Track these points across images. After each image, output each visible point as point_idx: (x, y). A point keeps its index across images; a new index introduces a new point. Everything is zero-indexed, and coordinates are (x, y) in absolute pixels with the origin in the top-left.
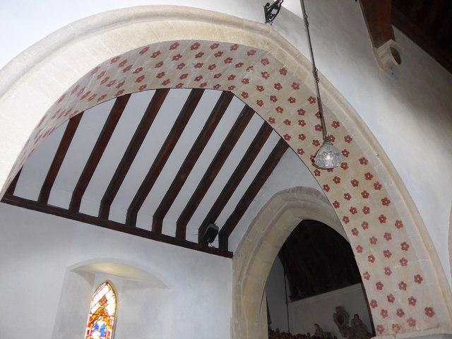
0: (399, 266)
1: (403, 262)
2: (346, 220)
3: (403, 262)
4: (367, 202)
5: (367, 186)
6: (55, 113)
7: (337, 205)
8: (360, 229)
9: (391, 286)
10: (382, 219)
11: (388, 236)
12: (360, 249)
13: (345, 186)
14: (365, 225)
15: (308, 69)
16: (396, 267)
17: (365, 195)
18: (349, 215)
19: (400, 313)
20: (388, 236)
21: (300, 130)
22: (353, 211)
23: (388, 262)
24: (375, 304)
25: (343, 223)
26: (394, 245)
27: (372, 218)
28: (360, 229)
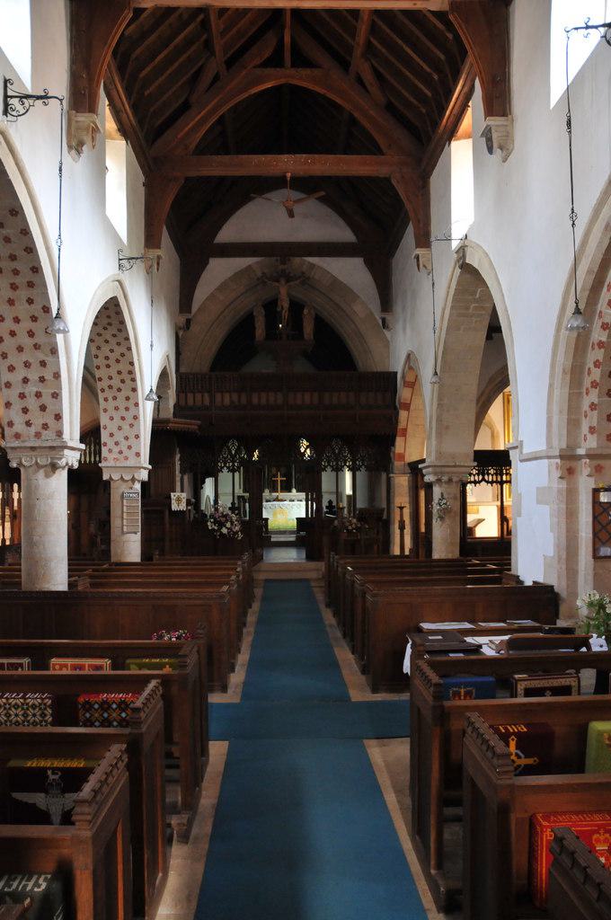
0: (128, 427)
1: (131, 425)
2: (103, 390)
3: (131, 425)
4: (121, 385)
5: (125, 376)
6: (398, 308)
7: (100, 379)
8: (110, 399)
9: (119, 436)
10: (128, 399)
11: (127, 409)
12: (105, 428)
13: (113, 372)
14: (115, 398)
15: (491, 428)
16: (126, 427)
17: (123, 381)
18: (107, 389)
19: (121, 452)
20: (127, 409)
21: (115, 431)
22: (110, 387)
23: (121, 423)
24: (105, 444)
25: (99, 392)
26: (129, 416)
27: (121, 396)
28: (110, 399)
